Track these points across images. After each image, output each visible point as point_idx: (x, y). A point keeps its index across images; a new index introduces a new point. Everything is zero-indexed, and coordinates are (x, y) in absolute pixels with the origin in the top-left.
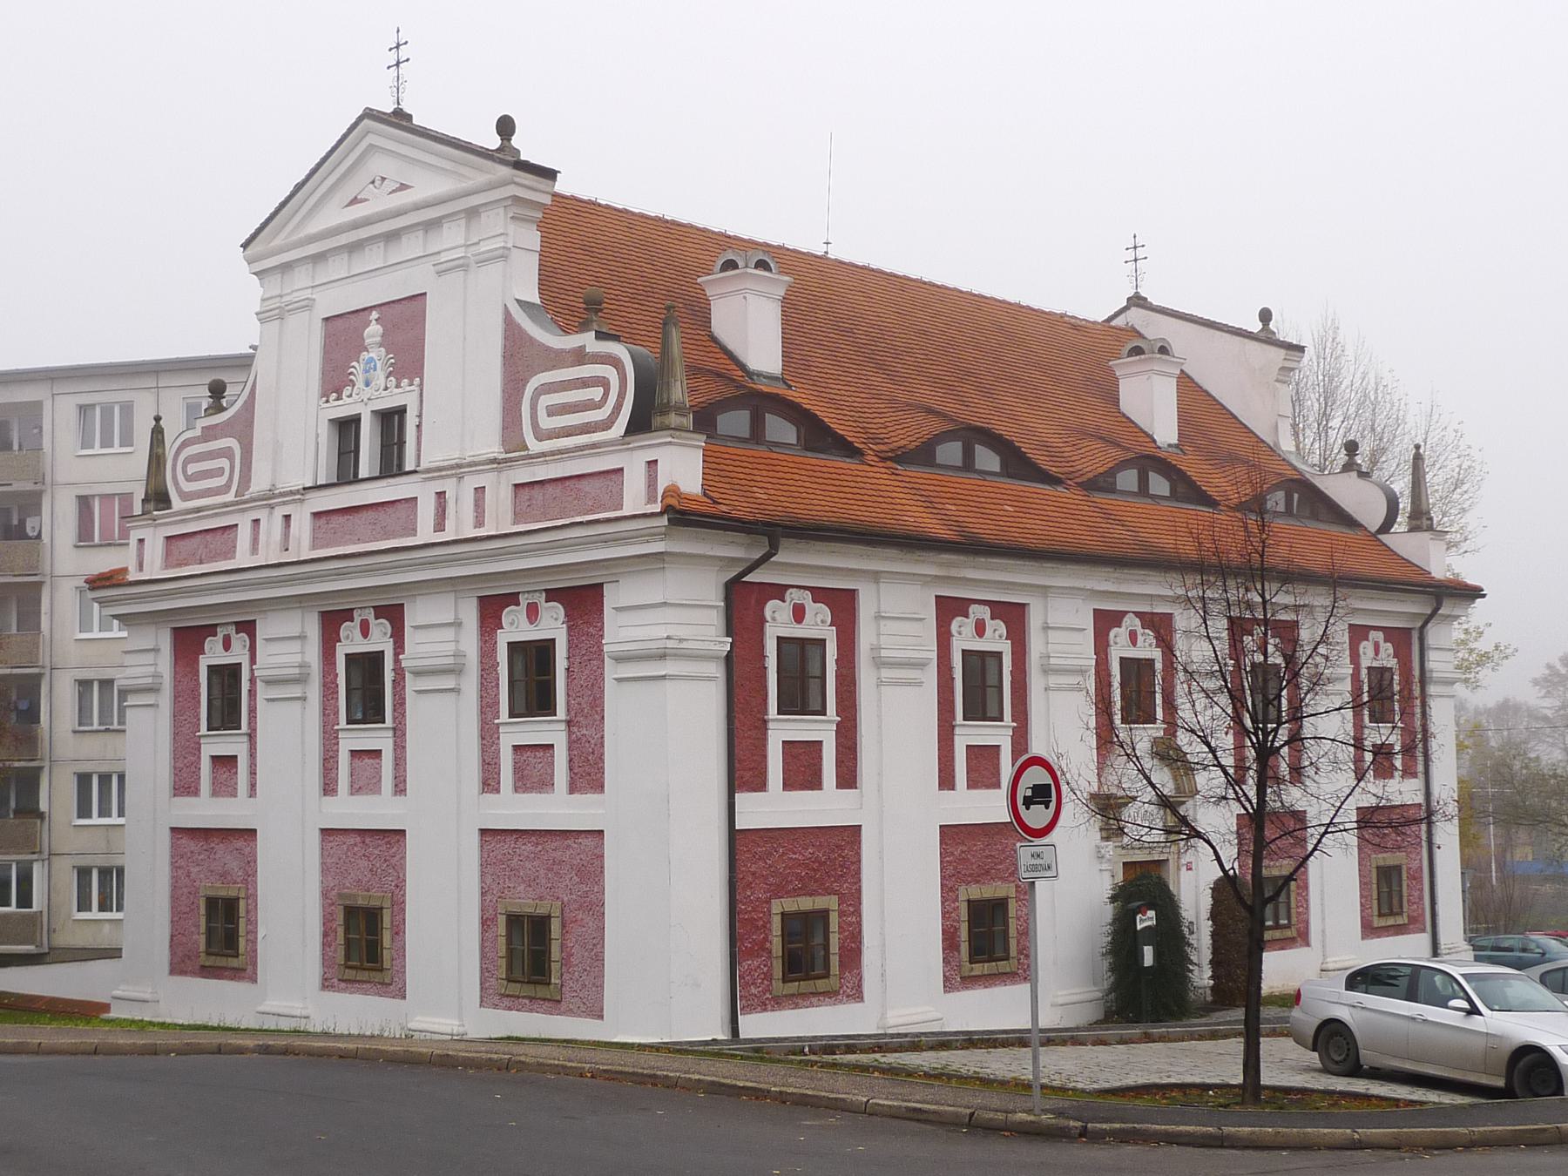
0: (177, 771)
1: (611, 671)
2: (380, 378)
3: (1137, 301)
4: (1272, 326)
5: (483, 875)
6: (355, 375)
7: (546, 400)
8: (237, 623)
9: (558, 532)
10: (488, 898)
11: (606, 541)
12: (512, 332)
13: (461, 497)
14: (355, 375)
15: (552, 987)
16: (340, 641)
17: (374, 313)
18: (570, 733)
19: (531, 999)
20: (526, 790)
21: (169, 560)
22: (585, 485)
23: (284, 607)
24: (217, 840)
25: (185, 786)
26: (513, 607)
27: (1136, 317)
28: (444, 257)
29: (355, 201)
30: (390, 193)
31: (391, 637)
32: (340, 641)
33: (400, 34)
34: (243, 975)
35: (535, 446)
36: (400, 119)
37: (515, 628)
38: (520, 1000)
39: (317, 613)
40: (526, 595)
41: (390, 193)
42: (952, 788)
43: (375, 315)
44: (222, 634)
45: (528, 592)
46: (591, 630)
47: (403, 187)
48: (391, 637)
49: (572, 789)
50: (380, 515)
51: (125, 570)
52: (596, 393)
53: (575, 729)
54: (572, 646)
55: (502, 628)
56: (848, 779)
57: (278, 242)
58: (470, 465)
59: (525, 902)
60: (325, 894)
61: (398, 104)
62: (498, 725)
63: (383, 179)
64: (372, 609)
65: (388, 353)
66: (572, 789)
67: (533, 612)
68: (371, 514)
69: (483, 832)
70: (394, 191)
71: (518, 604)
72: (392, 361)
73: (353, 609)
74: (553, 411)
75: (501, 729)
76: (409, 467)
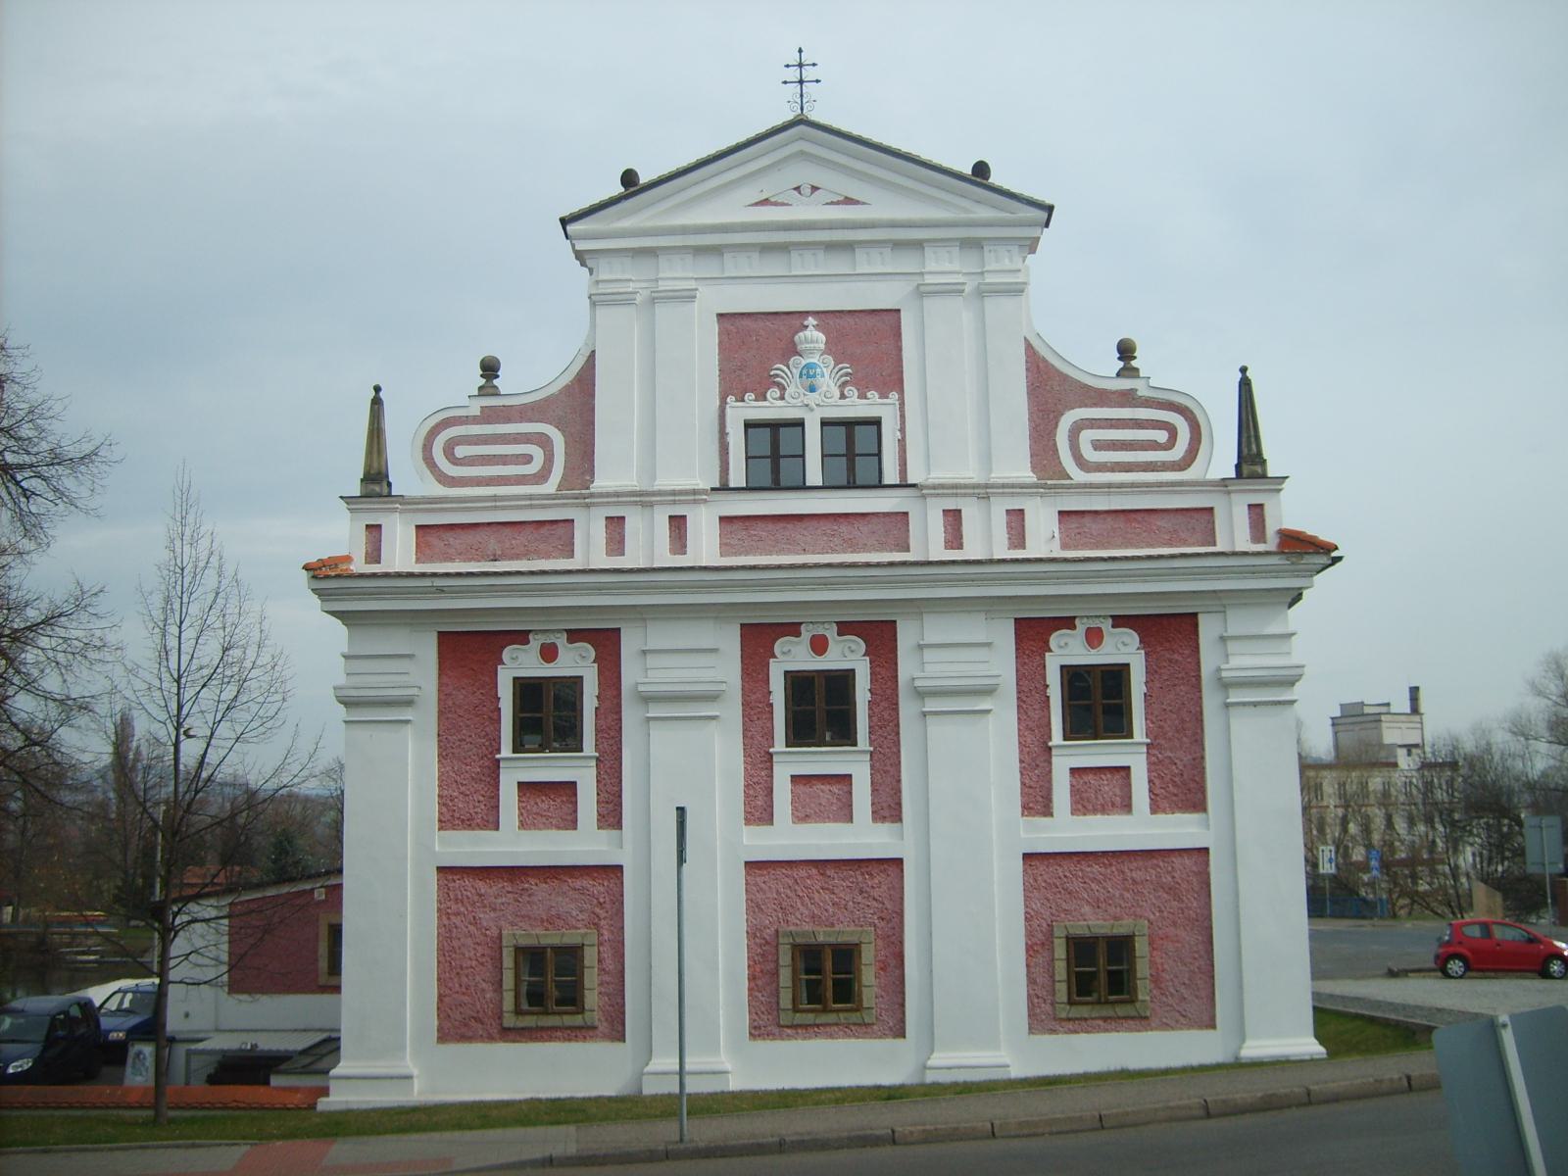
5: (1027, 898)
6: (782, 378)
7: (1087, 436)
8: (569, 632)
9: (1080, 564)
10: (1035, 923)
14: (782, 378)
15: (1138, 1005)
16: (774, 656)
19: (1105, 1019)
21: (423, 551)
23: (595, 617)
25: (759, 811)
26: (1069, 631)
28: (929, 279)
29: (765, 202)
30: (827, 204)
31: (594, 662)
32: (774, 656)
33: (803, 54)
34: (869, 1030)
35: (1079, 476)
38: (1089, 1022)
39: (436, 634)
40: (1085, 620)
42: (1047, 811)
43: (811, 321)
44: (1085, 627)
45: (1087, 617)
47: (849, 201)
48: (594, 662)
49: (1155, 808)
51: (348, 559)
52: (1162, 436)
54: (1151, 672)
55: (775, 657)
56: (611, 815)
58: (934, 487)
59: (1093, 922)
60: (752, 934)
62: (498, 761)
63: (814, 189)
64: (835, 625)
66: (1155, 808)
67: (819, 645)
71: (1074, 627)
72: (849, 370)
73: (1075, 618)
74: (1098, 445)
75: (1054, 752)
76: (891, 476)
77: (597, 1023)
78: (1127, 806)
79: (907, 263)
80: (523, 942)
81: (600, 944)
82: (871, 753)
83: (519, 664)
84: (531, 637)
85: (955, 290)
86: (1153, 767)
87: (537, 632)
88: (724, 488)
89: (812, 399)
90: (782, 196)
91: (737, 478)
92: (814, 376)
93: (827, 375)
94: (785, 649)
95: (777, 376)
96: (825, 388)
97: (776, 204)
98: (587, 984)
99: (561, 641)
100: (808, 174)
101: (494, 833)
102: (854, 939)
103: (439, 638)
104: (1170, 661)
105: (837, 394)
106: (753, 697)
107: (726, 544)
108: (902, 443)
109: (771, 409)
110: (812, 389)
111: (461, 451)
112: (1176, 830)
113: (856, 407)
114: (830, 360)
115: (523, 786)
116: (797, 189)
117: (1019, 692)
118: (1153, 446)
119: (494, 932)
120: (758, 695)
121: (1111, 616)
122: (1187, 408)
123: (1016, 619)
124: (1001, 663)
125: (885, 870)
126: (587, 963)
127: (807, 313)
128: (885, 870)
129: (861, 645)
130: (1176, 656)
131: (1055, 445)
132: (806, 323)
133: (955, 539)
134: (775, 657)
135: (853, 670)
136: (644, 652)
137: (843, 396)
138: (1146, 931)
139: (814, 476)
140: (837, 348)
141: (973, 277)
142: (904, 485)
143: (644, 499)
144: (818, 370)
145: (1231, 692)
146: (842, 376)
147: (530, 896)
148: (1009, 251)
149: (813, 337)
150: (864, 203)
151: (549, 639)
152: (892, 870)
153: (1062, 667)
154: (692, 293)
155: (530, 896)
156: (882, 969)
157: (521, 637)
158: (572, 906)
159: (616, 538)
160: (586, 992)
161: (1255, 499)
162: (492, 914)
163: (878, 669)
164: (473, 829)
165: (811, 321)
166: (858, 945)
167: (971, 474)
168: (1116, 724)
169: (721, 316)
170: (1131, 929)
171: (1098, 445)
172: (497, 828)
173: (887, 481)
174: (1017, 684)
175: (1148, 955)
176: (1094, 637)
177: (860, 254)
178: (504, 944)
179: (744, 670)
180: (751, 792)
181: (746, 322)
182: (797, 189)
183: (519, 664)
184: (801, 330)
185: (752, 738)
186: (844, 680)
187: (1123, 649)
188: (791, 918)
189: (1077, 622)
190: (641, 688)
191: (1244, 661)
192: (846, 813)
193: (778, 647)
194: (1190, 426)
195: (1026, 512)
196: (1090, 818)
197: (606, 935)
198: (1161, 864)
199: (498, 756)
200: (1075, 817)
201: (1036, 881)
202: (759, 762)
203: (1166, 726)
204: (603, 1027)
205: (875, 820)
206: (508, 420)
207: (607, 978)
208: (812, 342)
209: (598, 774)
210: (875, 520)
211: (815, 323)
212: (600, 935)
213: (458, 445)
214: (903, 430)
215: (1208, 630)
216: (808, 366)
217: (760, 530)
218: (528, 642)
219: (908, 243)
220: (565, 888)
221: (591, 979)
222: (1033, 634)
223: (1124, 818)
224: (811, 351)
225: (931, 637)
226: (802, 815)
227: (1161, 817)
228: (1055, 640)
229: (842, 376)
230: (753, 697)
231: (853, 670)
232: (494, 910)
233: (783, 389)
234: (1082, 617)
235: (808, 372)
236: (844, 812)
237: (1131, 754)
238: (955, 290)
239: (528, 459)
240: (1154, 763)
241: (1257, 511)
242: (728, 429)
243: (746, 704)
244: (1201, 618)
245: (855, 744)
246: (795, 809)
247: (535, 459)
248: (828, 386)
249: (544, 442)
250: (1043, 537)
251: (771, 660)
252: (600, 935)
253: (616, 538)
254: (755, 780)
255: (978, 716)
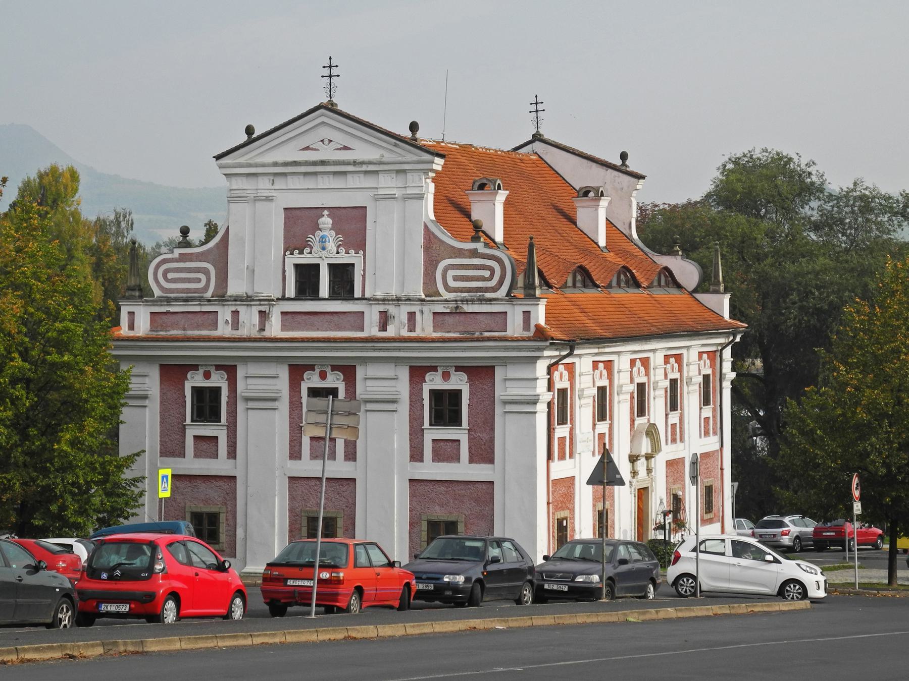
0: (291, 447)
1: (499, 410)
2: (331, 246)
3: (537, 138)
4: (627, 162)
6: (311, 242)
7: (451, 273)
10: (414, 513)
11: (506, 349)
12: (429, 235)
13: (400, 313)
14: (311, 242)
16: (303, 380)
17: (326, 211)
18: (469, 434)
20: (197, 458)
22: (479, 317)
24: (199, 482)
25: (416, 455)
26: (434, 373)
27: (538, 146)
28: (381, 192)
29: (307, 148)
30: (336, 149)
31: (343, 381)
32: (303, 380)
36: (330, 107)
37: (434, 382)
39: (408, 368)
41: (336, 149)
43: (326, 212)
46: (485, 386)
47: (346, 148)
48: (343, 381)
49: (471, 461)
50: (336, 318)
52: (487, 274)
53: (473, 433)
55: (188, 380)
56: (232, 453)
57: (242, 160)
61: (331, 97)
62: (423, 429)
63: (330, 141)
65: (337, 234)
66: (471, 461)
68: (328, 317)
69: (410, 480)
70: (338, 149)
72: (342, 239)
74: (456, 278)
75: (425, 431)
76: (357, 293)
77: (225, 549)
78: (458, 459)
79: (369, 182)
80: (195, 510)
81: (227, 512)
82: (469, 430)
83: (195, 380)
84: (199, 367)
85: (392, 198)
86: (471, 441)
87: (202, 365)
88: (284, 298)
89: (324, 254)
90: (314, 145)
91: (291, 292)
92: (325, 242)
93: (331, 241)
94: (308, 377)
95: (309, 241)
96: (330, 248)
97: (312, 149)
98: (221, 530)
99: (212, 370)
100: (326, 133)
101: (183, 459)
102: (334, 515)
103: (410, 369)
104: (482, 389)
105: (335, 250)
106: (294, 399)
107: (284, 325)
108: (364, 276)
109: (305, 259)
110: (324, 249)
111: (170, 276)
112: (479, 472)
113: (343, 259)
114: (333, 233)
115: (196, 437)
116: (322, 141)
117: (410, 401)
118: (483, 279)
119: (183, 505)
120: (296, 398)
121: (331, 365)
122: (501, 259)
123: (410, 366)
124: (402, 387)
125: (349, 484)
126: (221, 521)
127: (325, 208)
128: (349, 484)
129: (465, 377)
130: (485, 386)
131: (435, 278)
132: (323, 214)
133: (236, 325)
134: (188, 380)
135: (461, 390)
136: (506, 380)
137: (338, 253)
138: (463, 520)
139: (324, 291)
140: (336, 227)
141: (401, 189)
142: (363, 298)
143: (247, 300)
144: (327, 239)
145: (507, 406)
146: (338, 242)
147: (198, 489)
148: (359, 177)
149: (326, 221)
150: (353, 149)
151: (208, 369)
152: (351, 483)
153: (430, 390)
154: (422, 196)
155: (198, 489)
156: (346, 530)
157: (195, 368)
158: (216, 494)
159: (385, 320)
160: (221, 534)
161: (526, 308)
162: (182, 497)
163: (349, 388)
164: (174, 457)
165: (326, 212)
166: (336, 518)
167: (394, 292)
168: (454, 420)
169: (285, 209)
170: (457, 518)
171: (456, 278)
172: (422, 461)
173: (356, 296)
174: (410, 398)
175: (464, 532)
176: (446, 376)
177: (349, 176)
178: (186, 510)
179: (290, 386)
180: (293, 444)
181: (298, 212)
182: (322, 141)
183: (195, 380)
184: (321, 217)
185: (293, 418)
186: (217, 391)
187: (459, 382)
188: (309, 505)
189: (316, 367)
190: (502, 397)
191: (516, 391)
192: (456, 458)
193: (189, 375)
194: (157, 274)
195: (240, 313)
196: (441, 464)
197: (230, 508)
198: (472, 488)
199: (423, 427)
200: (434, 463)
201: (415, 493)
202: (416, 433)
203: (479, 421)
204: (227, 550)
205: (345, 460)
206: (191, 261)
207: (229, 528)
208: (325, 224)
209: (228, 432)
210: (349, 315)
211: (328, 213)
212: (227, 508)
213: (169, 272)
214: (364, 270)
215: (499, 373)
216: (323, 237)
217: (299, 318)
218: (198, 370)
219: (369, 169)
220: (212, 485)
221: (223, 528)
222: (418, 373)
223: (457, 464)
224: (325, 229)
225: (510, 375)
226: (314, 456)
227: (473, 465)
228: (428, 377)
229: (338, 242)
230: (294, 399)
231: (461, 390)
232: (183, 495)
233: (311, 248)
234: (441, 366)
235: (323, 240)
236: (456, 458)
237: (460, 434)
238: (392, 198)
239: (199, 280)
240: (472, 439)
241: (527, 314)
242: (286, 269)
243: (291, 402)
244: (496, 368)
245: (220, 421)
246: (311, 454)
247: (202, 281)
248: (332, 247)
249: (206, 272)
250: (425, 327)
251: (302, 382)
252: (227, 508)
253: (385, 320)
254: (295, 438)
255: (531, 415)
